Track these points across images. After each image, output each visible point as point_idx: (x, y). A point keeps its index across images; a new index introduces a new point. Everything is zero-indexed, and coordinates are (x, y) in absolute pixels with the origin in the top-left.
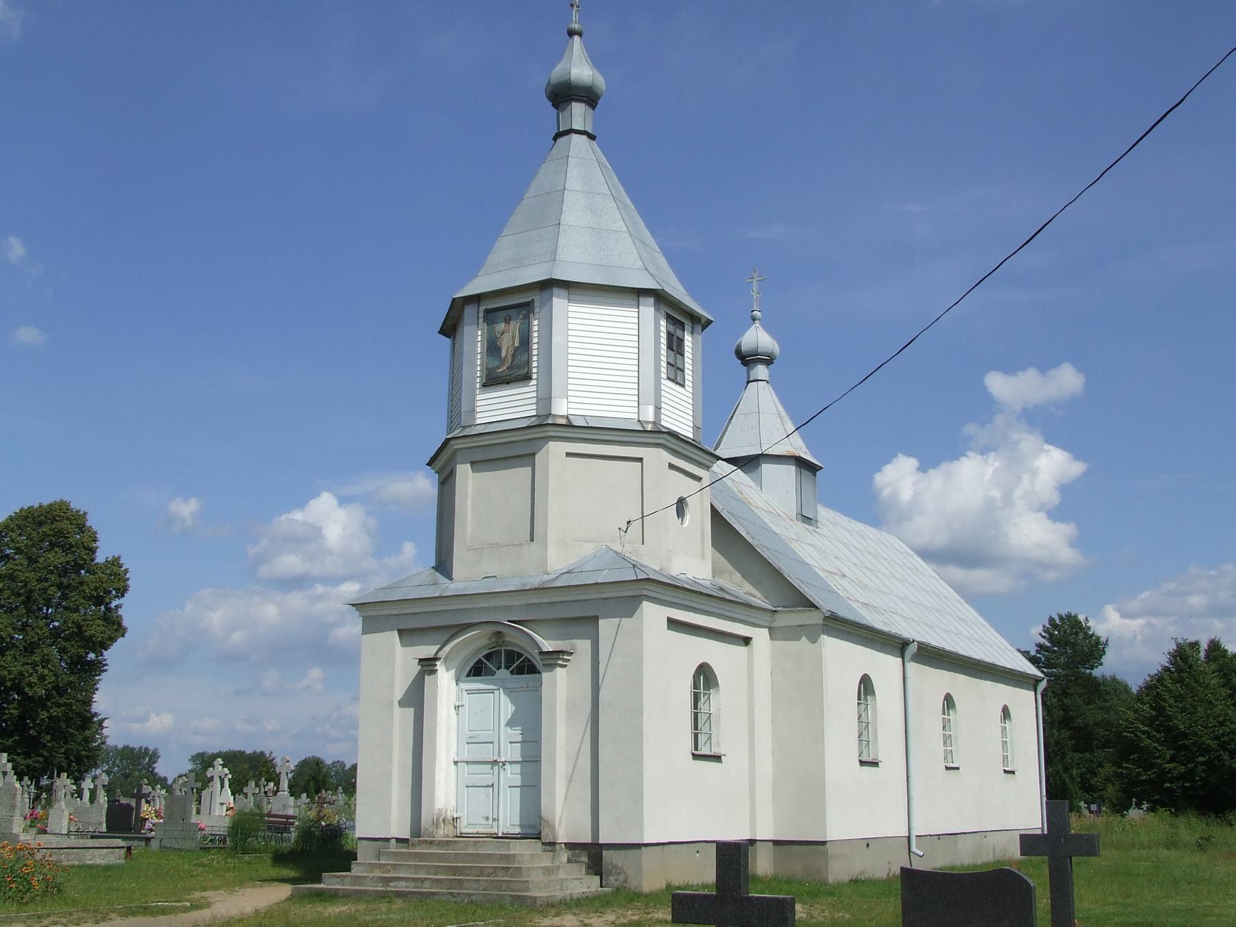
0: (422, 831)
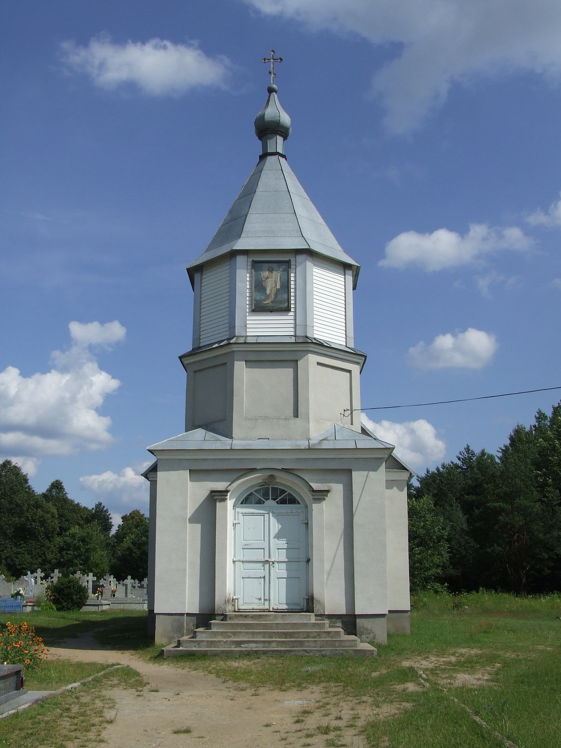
0: (216, 608)
